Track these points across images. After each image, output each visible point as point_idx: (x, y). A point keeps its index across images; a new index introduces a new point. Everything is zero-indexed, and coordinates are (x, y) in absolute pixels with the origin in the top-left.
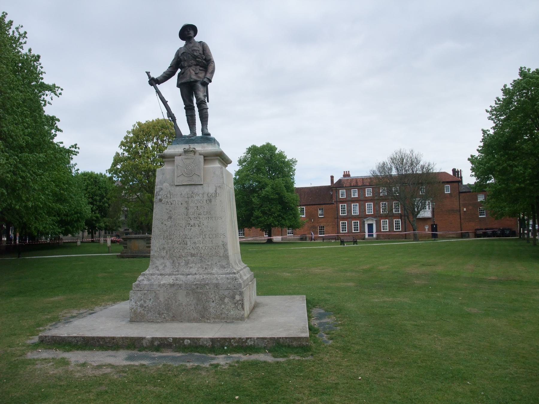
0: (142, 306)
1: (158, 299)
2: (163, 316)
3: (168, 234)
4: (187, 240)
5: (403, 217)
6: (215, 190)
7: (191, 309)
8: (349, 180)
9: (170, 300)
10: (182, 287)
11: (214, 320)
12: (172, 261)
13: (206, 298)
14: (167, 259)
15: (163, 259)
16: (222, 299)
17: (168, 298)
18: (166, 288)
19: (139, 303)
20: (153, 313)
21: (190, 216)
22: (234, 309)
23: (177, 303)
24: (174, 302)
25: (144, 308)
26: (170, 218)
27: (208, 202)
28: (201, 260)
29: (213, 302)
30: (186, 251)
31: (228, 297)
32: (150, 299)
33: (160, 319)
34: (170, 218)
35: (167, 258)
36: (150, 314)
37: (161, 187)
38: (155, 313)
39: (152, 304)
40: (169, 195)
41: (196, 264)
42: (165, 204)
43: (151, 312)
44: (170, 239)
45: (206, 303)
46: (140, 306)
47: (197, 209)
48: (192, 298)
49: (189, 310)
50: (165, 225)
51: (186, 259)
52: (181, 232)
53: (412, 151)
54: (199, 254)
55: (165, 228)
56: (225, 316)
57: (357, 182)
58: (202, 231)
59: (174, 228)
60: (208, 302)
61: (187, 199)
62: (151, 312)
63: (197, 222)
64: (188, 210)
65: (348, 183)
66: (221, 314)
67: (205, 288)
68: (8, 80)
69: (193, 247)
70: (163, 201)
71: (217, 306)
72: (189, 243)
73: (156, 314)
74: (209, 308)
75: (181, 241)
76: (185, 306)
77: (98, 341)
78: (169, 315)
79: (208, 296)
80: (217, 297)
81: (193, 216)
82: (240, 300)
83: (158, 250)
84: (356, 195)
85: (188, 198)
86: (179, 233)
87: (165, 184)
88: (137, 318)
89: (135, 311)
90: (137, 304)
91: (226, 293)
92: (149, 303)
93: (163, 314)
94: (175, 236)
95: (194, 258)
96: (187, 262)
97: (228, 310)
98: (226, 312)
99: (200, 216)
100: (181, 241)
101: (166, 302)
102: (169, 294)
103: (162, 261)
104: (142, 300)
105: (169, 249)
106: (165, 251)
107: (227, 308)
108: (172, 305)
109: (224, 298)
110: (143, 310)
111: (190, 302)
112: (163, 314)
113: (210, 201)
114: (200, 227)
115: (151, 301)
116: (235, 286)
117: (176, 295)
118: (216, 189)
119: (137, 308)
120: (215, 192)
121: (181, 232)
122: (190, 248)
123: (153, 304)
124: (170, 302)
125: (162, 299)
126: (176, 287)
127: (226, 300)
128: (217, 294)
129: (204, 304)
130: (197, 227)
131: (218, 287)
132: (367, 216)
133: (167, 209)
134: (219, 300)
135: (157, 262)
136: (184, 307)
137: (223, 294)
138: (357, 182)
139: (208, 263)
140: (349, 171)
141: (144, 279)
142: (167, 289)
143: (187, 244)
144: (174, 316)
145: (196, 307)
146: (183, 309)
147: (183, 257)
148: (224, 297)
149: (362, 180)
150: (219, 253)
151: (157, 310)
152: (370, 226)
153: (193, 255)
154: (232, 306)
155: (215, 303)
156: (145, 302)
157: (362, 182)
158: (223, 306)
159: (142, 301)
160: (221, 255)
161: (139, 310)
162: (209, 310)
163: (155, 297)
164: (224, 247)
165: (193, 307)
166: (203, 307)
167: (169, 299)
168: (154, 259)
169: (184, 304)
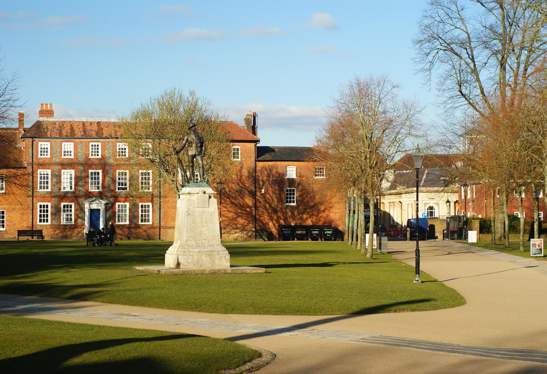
0: (186, 262)
5: (156, 200)
8: (57, 124)
16: (221, 258)
24: (200, 259)
30: (201, 238)
34: (194, 222)
40: (193, 212)
53: (192, 93)
55: (192, 227)
57: (72, 129)
63: (206, 225)
65: (55, 130)
68: (164, 172)
72: (203, 234)
84: (46, 147)
87: (191, 207)
91: (223, 255)
92: (190, 260)
97: (223, 263)
103: (191, 242)
113: (212, 215)
127: (223, 259)
132: (88, 195)
138: (72, 129)
140: (51, 105)
149: (81, 125)
152: (94, 213)
153: (205, 240)
156: (188, 260)
157: (81, 129)
161: (185, 263)
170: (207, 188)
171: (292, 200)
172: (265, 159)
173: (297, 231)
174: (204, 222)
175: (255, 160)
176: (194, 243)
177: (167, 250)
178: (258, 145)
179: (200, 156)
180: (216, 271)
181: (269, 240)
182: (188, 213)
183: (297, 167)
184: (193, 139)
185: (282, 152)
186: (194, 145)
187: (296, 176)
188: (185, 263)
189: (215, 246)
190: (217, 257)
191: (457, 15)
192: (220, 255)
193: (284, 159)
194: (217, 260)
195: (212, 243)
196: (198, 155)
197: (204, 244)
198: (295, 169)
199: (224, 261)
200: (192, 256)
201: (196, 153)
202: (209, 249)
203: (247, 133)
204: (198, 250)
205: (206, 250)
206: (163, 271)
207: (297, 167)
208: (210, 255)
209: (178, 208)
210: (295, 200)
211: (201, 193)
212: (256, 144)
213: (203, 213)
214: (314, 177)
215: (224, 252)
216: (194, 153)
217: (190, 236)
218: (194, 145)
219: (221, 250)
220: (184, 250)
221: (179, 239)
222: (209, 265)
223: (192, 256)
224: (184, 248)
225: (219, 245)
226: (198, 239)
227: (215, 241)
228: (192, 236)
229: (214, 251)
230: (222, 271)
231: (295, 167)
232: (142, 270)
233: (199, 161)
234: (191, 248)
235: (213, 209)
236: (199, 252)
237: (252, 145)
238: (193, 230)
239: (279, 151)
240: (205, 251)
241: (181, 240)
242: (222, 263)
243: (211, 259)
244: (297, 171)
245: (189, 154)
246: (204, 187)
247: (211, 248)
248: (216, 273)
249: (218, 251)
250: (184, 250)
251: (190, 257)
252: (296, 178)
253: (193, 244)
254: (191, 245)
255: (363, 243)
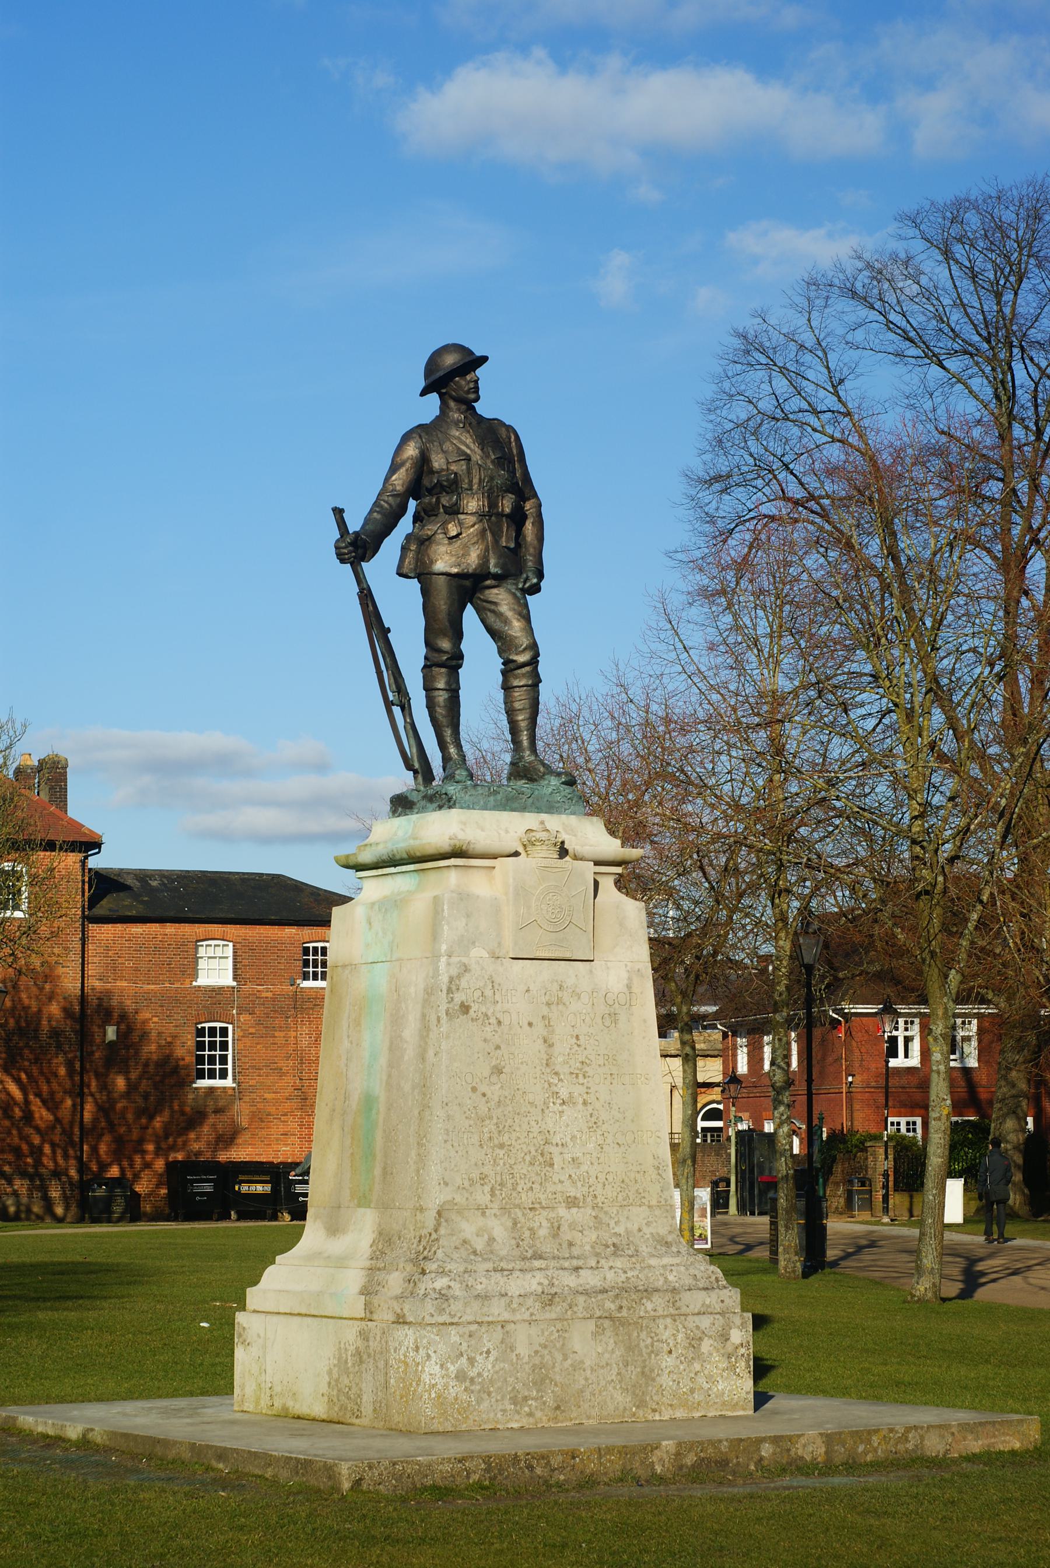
1: (512, 1349)
2: (527, 1409)
3: (493, 1128)
4: (552, 1149)
6: (626, 982)
7: (609, 1379)
9: (546, 1352)
10: (575, 1309)
11: (671, 1412)
12: (509, 1224)
13: (649, 1341)
14: (495, 1215)
15: (483, 1214)
16: (694, 1342)
17: (540, 1345)
18: (528, 1313)
19: (452, 1368)
20: (497, 1401)
21: (558, 1068)
22: (725, 1374)
23: (569, 1362)
24: (559, 1357)
25: (468, 1384)
26: (498, 1070)
27: (608, 1023)
28: (596, 1217)
29: (670, 1352)
31: (710, 1337)
32: (488, 1352)
33: (517, 1417)
34: (498, 1070)
35: (493, 1211)
36: (485, 1405)
37: (464, 960)
38: (503, 1399)
39: (494, 1366)
40: (488, 993)
41: (581, 1232)
42: (480, 1021)
43: (489, 1394)
44: (502, 1146)
45: (650, 1357)
46: (457, 1377)
47: (579, 1046)
48: (612, 1341)
49: (602, 1383)
50: (484, 1095)
51: (552, 1215)
52: (533, 1123)
54: (589, 1199)
55: (483, 1109)
56: (702, 1398)
58: (593, 1119)
59: (510, 1108)
60: (657, 1355)
61: (545, 1011)
62: (489, 1394)
63: (578, 1090)
64: (551, 1046)
66: (692, 1391)
67: (643, 1308)
69: (570, 1176)
70: (471, 1011)
71: (682, 1367)
72: (557, 1160)
73: (507, 1402)
74: (658, 1375)
75: (533, 1153)
76: (592, 1370)
77: (530, 1468)
78: (544, 1403)
79: (657, 1335)
80: (680, 1337)
81: (567, 1070)
82: (742, 1345)
83: (467, 1184)
85: (548, 1004)
86: (525, 1127)
88: (447, 1420)
89: (439, 1396)
90: (447, 1369)
91: (705, 1322)
92: (485, 1366)
93: (526, 1399)
94: (514, 1135)
95: (574, 1210)
96: (556, 1224)
97: (710, 1378)
98: (706, 1386)
99: (587, 1069)
100: (533, 1153)
101: (537, 1360)
102: (546, 1333)
104: (462, 1355)
105: (499, 1179)
106: (487, 1189)
107: (706, 1372)
108: (554, 1367)
109: (701, 1339)
110: (466, 1390)
111: (607, 1356)
112: (526, 1399)
113: (614, 1016)
114: (590, 1108)
115: (491, 1358)
116: (722, 1301)
117: (566, 1335)
118: (630, 979)
119: (446, 1386)
120: (625, 990)
121: (533, 1123)
122: (562, 1179)
123: (497, 1368)
124: (547, 1357)
125: (523, 1350)
126: (559, 1308)
127: (706, 1346)
128: (680, 1327)
129: (645, 1360)
130: (580, 1107)
131: (678, 1304)
133: (485, 1040)
134: (685, 1348)
135: (464, 1225)
136: (588, 1372)
137: (698, 1327)
139: (617, 1230)
141: (452, 1284)
142: (532, 1314)
143: (552, 1165)
144: (558, 1408)
145: (623, 1371)
146: (586, 1379)
147: (543, 1208)
148: (700, 1335)
150: (646, 1195)
151: (510, 1389)
153: (572, 1202)
154: (720, 1365)
155: (674, 1355)
156: (472, 1361)
158: (697, 1366)
159: (464, 1360)
160: (654, 1202)
161: (455, 1390)
162: (658, 1378)
163: (502, 1342)
164: (659, 1174)
165: (615, 1371)
166: (643, 1373)
167: (545, 1347)
168: (453, 1217)
169: (588, 1363)
170: (573, 820)
171: (218, 1067)
172: (120, 913)
173: (241, 1182)
174: (563, 1070)
175: (84, 917)
176: (499, 1229)
177: (255, 1282)
178: (94, 862)
179: (510, 584)
180: (724, 1447)
181: (80, 1220)
182: (459, 997)
183: (238, 946)
184: (468, 459)
185: (177, 889)
186: (473, 504)
187: (235, 979)
188: (455, 1390)
189: (644, 1249)
190: (666, 1331)
191: (831, 402)
192: (692, 1322)
193: (190, 915)
194: (669, 1361)
195: (620, 1229)
196: (500, 579)
197: (566, 1235)
198: (229, 951)
199: (717, 1362)
200: (498, 1334)
201: (484, 559)
202: (610, 1275)
203: (52, 814)
204: (533, 1283)
205: (590, 1279)
206: (344, 1469)
207: (238, 946)
208: (623, 1323)
209: (350, 966)
210: (230, 1066)
211: (545, 855)
212: (86, 858)
213: (560, 1001)
214: (298, 981)
215: (711, 1299)
216: (473, 559)
217: (475, 1175)
218: (473, 504)
219: (688, 1281)
220: (441, 1283)
221: (363, 1201)
222: (619, 1399)
223: (498, 1334)
224: (442, 1272)
225: (668, 1244)
226: (526, 1199)
227: (638, 1216)
228: (483, 1178)
229: (649, 1292)
230: (766, 1450)
231: (231, 944)
232: (84, 1443)
233: (506, 621)
234: (482, 1267)
235: (625, 975)
236: (549, 1299)
237: (72, 859)
238: (490, 1126)
239: (164, 884)
240: (586, 1293)
241: (385, 1207)
242: (701, 1380)
243: (630, 1349)
244: (239, 959)
245: (440, 566)
246: (551, 808)
247: (619, 1263)
248: (723, 1463)
249: (674, 1290)
250: (441, 1283)
251: (490, 1340)
252: (235, 984)
253: (492, 1240)
254: (479, 1244)
255: (787, 1228)
